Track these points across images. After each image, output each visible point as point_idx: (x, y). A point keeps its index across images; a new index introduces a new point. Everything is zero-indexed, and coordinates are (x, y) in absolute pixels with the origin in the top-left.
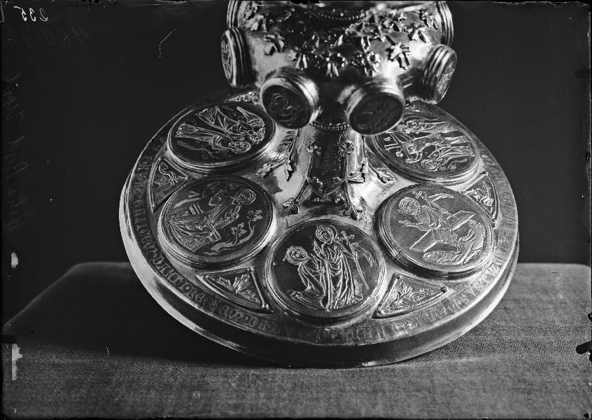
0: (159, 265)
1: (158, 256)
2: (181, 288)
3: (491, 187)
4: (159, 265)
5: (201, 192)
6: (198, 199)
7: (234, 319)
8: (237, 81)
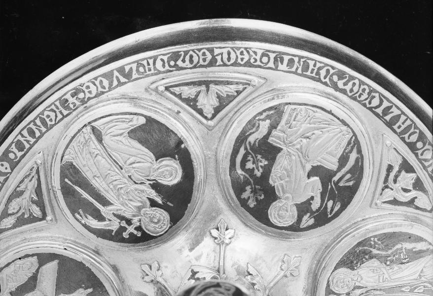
0: (320, 69)
1: (331, 80)
2: (272, 56)
3: (339, 169)
4: (320, 69)
5: (339, 189)
6: (336, 178)
7: (186, 53)
8: (66, 183)
